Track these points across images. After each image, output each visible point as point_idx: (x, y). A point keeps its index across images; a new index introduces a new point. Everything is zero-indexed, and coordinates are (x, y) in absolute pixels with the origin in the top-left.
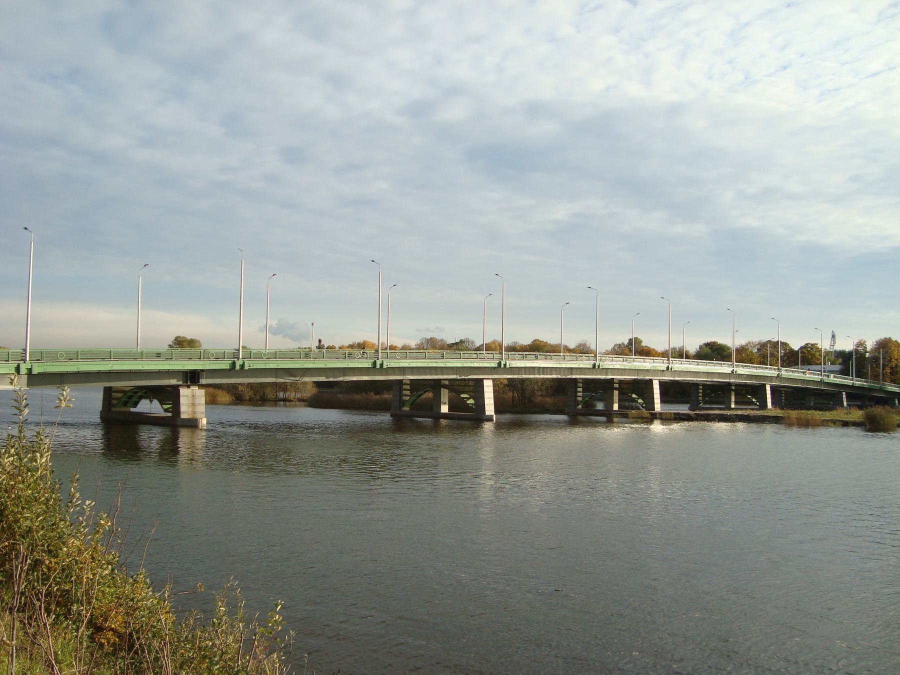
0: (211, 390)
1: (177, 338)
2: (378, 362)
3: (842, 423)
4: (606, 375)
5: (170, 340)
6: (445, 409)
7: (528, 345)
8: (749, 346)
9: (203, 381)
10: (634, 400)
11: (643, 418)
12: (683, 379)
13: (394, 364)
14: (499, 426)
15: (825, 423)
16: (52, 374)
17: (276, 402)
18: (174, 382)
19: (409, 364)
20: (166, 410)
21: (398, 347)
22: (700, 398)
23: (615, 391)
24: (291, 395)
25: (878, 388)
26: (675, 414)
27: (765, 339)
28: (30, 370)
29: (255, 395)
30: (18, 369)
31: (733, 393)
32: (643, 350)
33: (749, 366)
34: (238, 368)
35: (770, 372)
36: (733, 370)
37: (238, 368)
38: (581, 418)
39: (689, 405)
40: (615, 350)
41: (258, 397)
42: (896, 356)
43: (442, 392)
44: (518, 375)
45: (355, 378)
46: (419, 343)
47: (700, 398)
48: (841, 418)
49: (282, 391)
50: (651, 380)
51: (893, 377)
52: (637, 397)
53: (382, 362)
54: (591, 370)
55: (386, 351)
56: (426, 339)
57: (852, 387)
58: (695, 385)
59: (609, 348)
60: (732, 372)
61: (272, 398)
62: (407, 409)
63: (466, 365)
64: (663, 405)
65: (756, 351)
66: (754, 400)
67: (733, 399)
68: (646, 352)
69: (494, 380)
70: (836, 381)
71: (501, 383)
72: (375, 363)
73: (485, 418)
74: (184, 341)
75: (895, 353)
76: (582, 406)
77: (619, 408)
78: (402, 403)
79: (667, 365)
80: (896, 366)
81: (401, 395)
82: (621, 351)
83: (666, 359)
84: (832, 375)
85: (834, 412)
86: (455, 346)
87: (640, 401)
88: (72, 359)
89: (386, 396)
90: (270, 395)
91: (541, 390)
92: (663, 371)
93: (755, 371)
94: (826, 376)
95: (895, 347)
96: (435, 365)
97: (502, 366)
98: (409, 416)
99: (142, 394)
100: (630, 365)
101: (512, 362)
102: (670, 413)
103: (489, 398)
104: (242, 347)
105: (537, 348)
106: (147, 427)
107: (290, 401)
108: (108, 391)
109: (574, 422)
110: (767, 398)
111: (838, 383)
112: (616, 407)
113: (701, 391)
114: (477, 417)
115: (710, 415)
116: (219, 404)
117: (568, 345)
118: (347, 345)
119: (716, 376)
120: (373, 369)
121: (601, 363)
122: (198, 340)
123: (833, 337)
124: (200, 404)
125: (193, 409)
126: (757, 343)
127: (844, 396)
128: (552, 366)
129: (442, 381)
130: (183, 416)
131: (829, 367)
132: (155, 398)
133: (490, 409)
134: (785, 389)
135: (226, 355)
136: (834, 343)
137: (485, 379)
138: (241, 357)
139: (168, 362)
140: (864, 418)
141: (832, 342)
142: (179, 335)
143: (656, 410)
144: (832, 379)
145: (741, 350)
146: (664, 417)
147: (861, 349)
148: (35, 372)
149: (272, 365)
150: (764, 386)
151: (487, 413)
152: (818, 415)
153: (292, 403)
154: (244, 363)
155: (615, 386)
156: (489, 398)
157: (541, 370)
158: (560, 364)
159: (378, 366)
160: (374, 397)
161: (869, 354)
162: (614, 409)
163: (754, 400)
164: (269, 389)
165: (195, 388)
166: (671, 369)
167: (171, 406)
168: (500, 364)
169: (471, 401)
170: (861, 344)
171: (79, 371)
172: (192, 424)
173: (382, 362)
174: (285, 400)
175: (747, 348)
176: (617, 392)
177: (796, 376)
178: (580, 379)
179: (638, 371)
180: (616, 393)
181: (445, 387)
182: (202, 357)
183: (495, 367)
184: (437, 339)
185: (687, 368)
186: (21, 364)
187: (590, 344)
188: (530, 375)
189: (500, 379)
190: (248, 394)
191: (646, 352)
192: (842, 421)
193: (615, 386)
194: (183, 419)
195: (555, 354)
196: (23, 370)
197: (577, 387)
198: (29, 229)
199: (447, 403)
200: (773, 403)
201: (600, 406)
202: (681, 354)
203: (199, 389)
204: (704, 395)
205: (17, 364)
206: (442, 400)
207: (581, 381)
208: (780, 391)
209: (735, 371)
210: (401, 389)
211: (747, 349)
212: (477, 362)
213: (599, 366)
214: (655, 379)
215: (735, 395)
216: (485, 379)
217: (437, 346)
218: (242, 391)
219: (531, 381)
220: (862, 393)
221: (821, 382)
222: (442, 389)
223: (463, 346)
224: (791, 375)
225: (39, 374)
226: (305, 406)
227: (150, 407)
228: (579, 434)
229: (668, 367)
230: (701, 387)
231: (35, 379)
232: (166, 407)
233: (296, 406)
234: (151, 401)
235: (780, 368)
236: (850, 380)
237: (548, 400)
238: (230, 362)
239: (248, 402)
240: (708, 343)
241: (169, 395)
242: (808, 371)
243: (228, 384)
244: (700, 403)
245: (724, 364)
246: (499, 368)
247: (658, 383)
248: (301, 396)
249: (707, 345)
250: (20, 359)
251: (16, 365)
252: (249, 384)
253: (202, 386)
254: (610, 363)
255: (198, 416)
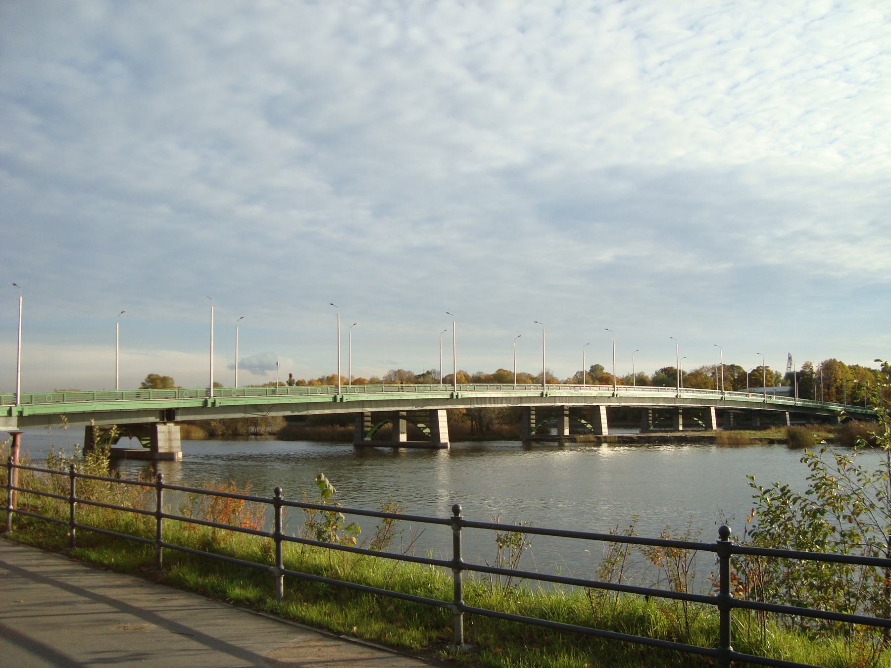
0: (186, 426)
1: (150, 376)
2: (339, 397)
3: (768, 441)
4: (554, 403)
5: (143, 378)
6: (403, 438)
7: (492, 375)
8: (703, 370)
9: (179, 418)
10: (583, 426)
11: (590, 442)
12: (641, 404)
13: (353, 398)
14: (453, 454)
15: (752, 442)
16: (74, 414)
17: (247, 436)
18: (152, 419)
19: (367, 398)
20: (145, 446)
21: (366, 380)
22: (650, 422)
23: (565, 417)
24: (262, 429)
25: (819, 407)
26: (619, 437)
27: (717, 363)
28: (21, 413)
29: (227, 430)
30: (10, 412)
31: (681, 416)
32: (602, 377)
33: (706, 391)
34: (209, 405)
35: (715, 395)
36: (677, 395)
37: (209, 405)
38: (534, 444)
39: (640, 429)
40: (577, 377)
41: (230, 432)
42: (841, 377)
43: (400, 423)
44: (470, 404)
45: (317, 412)
46: (387, 375)
47: (650, 422)
48: (769, 436)
49: (253, 426)
50: (598, 407)
51: (838, 396)
52: (586, 422)
53: (342, 397)
54: (539, 398)
55: (346, 386)
56: (394, 371)
57: (795, 407)
58: (645, 410)
59: (571, 375)
60: (677, 396)
61: (243, 432)
62: (368, 439)
63: (420, 397)
64: (611, 430)
65: (711, 374)
66: (700, 422)
67: (681, 422)
68: (605, 380)
69: (448, 410)
70: (779, 402)
71: (460, 412)
72: (335, 398)
73: (440, 446)
74: (156, 379)
75: (840, 373)
76: (536, 433)
77: (570, 433)
78: (365, 434)
79: (612, 392)
80: (842, 386)
81: (363, 426)
82: (578, 380)
83: (612, 386)
84: (774, 396)
85: (768, 431)
86: (422, 377)
87: (589, 426)
88: (118, 399)
89: (351, 428)
90: (242, 430)
91: (497, 418)
92: (609, 397)
93: (699, 395)
94: (768, 397)
95: (839, 367)
96: (391, 398)
97: (455, 397)
98: (371, 445)
99: (123, 432)
100: (577, 392)
101: (464, 393)
102: (615, 436)
103: (444, 427)
104: (214, 383)
105: (501, 378)
106: (126, 462)
107: (261, 435)
108: (89, 430)
109: (528, 447)
110: (712, 423)
111: (780, 403)
112: (567, 432)
113: (651, 415)
114: (432, 445)
115: (651, 437)
116: (192, 440)
117: (531, 374)
118: (317, 379)
119: (661, 400)
120: (334, 403)
121: (549, 392)
122: (170, 377)
123: (790, 358)
124: (176, 439)
125: (170, 444)
126: (711, 367)
127: (788, 416)
128: (502, 396)
129: (401, 413)
130: (161, 451)
131: (780, 388)
132: (134, 435)
133: (444, 437)
134: (734, 411)
135: (198, 394)
136: (791, 364)
137: (439, 409)
138: (212, 395)
139: (147, 402)
140: (787, 436)
141: (789, 364)
142: (152, 373)
143: (603, 434)
144: (775, 400)
145: (696, 374)
146: (608, 440)
147: (808, 370)
148: (25, 414)
149: (241, 402)
150: (709, 408)
151: (442, 441)
152: (748, 434)
153: (263, 437)
154: (215, 400)
155: (565, 413)
156: (444, 427)
157: (492, 399)
158: (509, 393)
159: (338, 400)
160: (339, 429)
161: (816, 375)
162: (565, 434)
163: (700, 422)
164: (241, 423)
165: (171, 425)
166: (617, 395)
167: (149, 441)
168: (452, 395)
169: (427, 431)
170: (807, 366)
171: (65, 412)
172: (169, 457)
173: (342, 397)
174: (256, 434)
175: (701, 372)
176: (568, 418)
177: (740, 398)
178: (533, 407)
179: (585, 398)
180: (566, 419)
181: (403, 417)
182: (177, 396)
183: (448, 398)
184: (404, 371)
185: (632, 394)
186: (12, 408)
187: (552, 373)
188: (482, 404)
189: (459, 408)
190: (220, 430)
191: (605, 380)
192: (769, 439)
193: (565, 413)
194: (160, 453)
195: (504, 384)
196: (15, 413)
197: (530, 415)
198: (17, 285)
199: (406, 432)
200: (718, 425)
201: (554, 432)
202: (641, 381)
203: (174, 425)
204: (654, 420)
205: (9, 408)
206: (401, 430)
207: (534, 409)
208: (729, 413)
209: (679, 395)
210: (363, 421)
211: (701, 374)
212: (431, 394)
213: (546, 395)
214: (601, 405)
215: (683, 418)
216: (439, 409)
217: (405, 378)
218: (215, 427)
219: (487, 409)
220: (806, 412)
221: (764, 403)
222: (400, 420)
223: (430, 377)
224: (734, 398)
225: (30, 416)
226: (275, 439)
227: (132, 444)
228: (532, 457)
229: (614, 393)
230: (650, 411)
231: (23, 420)
232: (144, 442)
233: (266, 439)
234: (130, 438)
235: (724, 391)
236: (792, 400)
237: (506, 427)
238: (203, 400)
239: (220, 437)
240: (664, 368)
241: (148, 432)
242: (750, 394)
243: (201, 420)
244: (650, 427)
245: (668, 389)
246: (452, 399)
247: (605, 408)
248: (272, 430)
249: (664, 370)
250: (11, 403)
251: (8, 408)
252: (221, 419)
253: (177, 423)
254: (557, 391)
255: (174, 450)
